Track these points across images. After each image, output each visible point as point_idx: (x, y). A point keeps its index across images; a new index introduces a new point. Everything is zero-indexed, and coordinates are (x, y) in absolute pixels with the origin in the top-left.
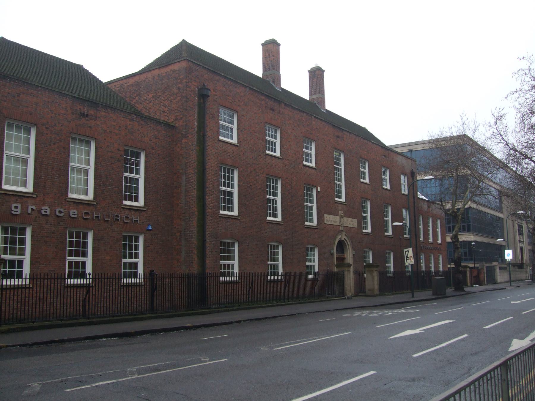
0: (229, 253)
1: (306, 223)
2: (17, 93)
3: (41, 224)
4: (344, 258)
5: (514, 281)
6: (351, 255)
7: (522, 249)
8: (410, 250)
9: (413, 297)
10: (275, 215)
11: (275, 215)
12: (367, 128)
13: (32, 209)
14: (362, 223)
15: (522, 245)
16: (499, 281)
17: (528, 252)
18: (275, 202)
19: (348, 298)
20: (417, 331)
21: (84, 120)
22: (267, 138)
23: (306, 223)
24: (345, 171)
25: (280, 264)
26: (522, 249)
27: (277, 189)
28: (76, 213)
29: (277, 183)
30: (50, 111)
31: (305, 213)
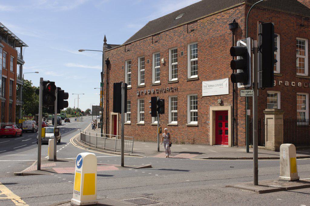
2: (271, 17)
3: (284, 91)
13: (281, 83)
21: (302, 28)
28: (301, 84)
30: (286, 25)
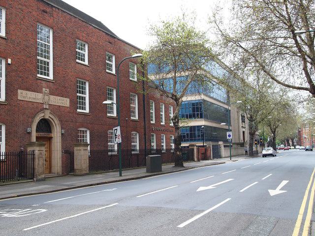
0: (83, 137)
1: (108, 115)
4: (51, 138)
5: (234, 156)
6: (59, 135)
7: (244, 132)
8: (119, 128)
9: (121, 175)
10: (84, 108)
11: (84, 108)
12: (102, 22)
14: (77, 102)
15: (244, 130)
16: (223, 156)
17: (249, 134)
18: (84, 98)
19: (38, 181)
20: (210, 187)
22: (77, 50)
23: (108, 115)
24: (53, 48)
25: (138, 144)
26: (244, 132)
27: (113, 96)
29: (113, 92)
31: (130, 112)
